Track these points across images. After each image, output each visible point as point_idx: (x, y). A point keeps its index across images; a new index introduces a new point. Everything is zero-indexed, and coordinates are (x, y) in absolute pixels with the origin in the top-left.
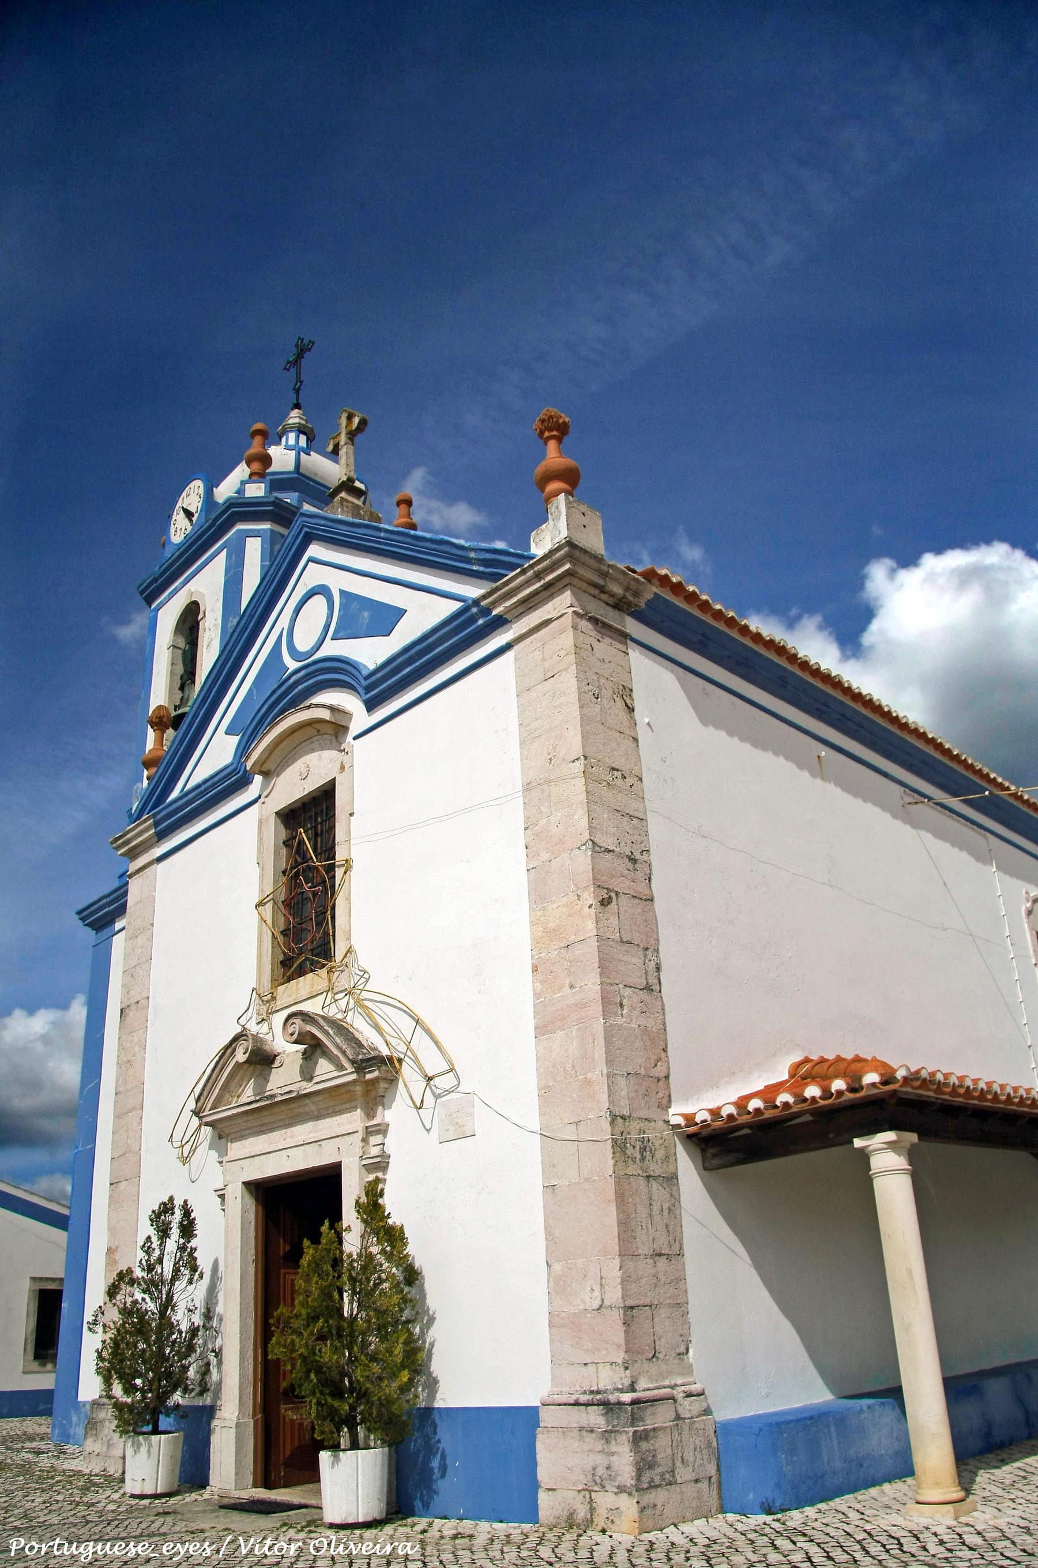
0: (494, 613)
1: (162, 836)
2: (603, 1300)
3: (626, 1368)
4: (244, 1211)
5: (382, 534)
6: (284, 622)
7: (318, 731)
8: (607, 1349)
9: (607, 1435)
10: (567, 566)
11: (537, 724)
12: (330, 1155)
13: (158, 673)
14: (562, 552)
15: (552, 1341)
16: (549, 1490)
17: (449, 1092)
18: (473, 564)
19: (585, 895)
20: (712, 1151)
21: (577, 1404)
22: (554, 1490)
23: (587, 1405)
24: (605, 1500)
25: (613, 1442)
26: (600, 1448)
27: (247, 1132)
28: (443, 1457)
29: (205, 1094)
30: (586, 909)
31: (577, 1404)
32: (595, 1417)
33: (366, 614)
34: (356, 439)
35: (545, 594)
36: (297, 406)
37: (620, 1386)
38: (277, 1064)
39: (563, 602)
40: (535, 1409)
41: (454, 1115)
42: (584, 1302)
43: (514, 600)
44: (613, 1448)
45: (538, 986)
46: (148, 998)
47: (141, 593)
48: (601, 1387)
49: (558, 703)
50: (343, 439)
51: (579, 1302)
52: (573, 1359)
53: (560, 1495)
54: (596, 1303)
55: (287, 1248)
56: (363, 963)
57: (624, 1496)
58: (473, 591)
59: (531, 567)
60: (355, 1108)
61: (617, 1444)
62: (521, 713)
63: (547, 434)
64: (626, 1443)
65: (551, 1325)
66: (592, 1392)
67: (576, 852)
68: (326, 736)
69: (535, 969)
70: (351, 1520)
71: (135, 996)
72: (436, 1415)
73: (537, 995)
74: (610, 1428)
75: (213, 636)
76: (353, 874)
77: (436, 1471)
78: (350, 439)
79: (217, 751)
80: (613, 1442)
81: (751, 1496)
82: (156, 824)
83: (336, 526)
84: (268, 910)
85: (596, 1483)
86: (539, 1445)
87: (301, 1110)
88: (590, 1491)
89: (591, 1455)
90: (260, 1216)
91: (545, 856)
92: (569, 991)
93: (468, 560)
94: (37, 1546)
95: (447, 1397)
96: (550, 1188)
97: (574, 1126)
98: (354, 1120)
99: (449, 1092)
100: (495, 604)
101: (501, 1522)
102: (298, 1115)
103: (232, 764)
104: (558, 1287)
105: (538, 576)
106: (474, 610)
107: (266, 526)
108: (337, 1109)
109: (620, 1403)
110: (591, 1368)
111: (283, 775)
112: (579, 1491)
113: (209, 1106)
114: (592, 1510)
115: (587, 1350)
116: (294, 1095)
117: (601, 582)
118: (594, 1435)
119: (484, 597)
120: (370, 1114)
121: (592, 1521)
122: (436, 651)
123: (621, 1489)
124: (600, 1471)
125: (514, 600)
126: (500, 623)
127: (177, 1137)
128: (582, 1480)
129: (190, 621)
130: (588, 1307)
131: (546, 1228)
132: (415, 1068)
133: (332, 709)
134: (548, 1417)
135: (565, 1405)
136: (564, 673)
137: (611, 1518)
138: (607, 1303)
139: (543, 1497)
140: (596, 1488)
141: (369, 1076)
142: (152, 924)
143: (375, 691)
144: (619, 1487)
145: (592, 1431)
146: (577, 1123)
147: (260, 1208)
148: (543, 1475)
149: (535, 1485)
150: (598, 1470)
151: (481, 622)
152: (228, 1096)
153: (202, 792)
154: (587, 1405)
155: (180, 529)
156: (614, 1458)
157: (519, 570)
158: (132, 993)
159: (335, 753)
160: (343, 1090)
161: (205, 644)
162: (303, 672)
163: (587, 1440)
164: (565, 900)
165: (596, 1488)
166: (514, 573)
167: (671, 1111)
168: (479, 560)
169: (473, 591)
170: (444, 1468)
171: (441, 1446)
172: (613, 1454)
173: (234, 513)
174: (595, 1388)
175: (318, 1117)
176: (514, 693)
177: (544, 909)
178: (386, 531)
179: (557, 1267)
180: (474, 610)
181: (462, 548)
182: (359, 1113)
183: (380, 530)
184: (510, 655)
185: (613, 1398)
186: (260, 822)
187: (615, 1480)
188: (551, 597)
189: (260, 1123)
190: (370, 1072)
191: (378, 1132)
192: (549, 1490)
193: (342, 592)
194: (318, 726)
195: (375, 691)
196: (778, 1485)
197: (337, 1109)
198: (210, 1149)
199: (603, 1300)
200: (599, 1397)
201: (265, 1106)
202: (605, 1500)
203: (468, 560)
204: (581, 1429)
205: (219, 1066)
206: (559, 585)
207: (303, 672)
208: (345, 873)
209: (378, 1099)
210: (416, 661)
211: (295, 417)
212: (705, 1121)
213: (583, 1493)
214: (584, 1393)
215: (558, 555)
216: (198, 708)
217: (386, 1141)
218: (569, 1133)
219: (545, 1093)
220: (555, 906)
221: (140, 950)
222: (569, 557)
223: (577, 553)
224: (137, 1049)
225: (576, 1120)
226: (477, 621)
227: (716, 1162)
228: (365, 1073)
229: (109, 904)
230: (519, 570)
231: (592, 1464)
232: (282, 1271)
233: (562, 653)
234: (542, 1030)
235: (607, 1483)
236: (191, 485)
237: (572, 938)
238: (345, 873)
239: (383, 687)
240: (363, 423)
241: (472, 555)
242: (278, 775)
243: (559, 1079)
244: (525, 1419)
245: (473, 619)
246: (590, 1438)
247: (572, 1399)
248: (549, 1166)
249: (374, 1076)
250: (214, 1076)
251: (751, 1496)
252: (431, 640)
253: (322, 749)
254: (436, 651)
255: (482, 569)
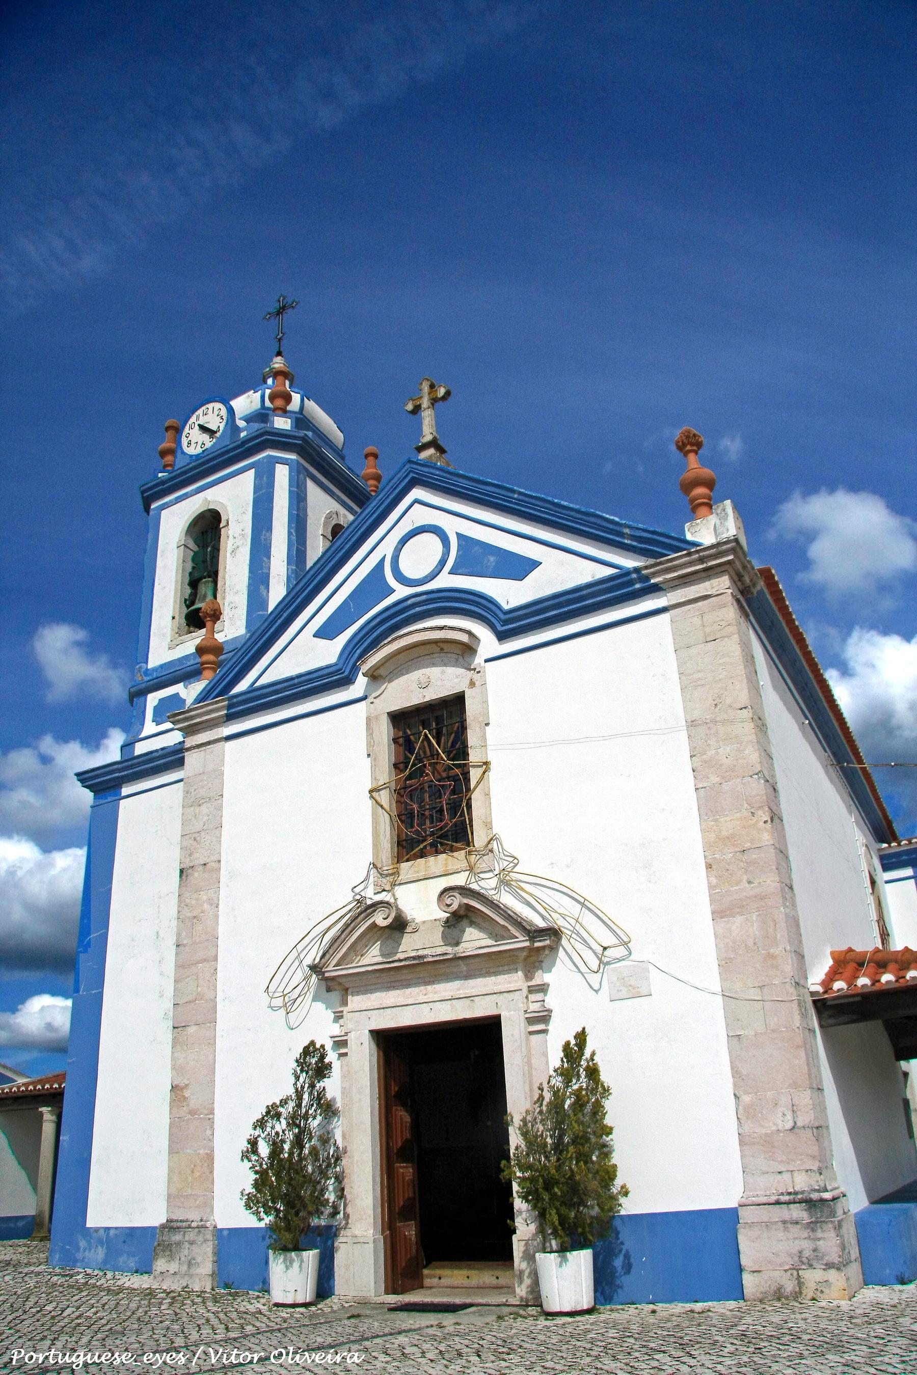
0: (652, 581)
1: (231, 717)
2: (795, 1123)
3: (821, 1174)
4: (371, 1055)
5: (516, 496)
6: (387, 549)
7: (442, 649)
8: (801, 1160)
9: (812, 1226)
10: (731, 557)
11: (700, 675)
12: (487, 1009)
13: (165, 567)
14: (729, 546)
15: (742, 1157)
16: (754, 1272)
17: (619, 960)
18: (624, 538)
19: (760, 812)
20: (827, 1013)
21: (778, 1203)
22: (759, 1271)
23: (788, 1203)
24: (813, 1276)
25: (819, 1230)
26: (806, 1235)
27: (373, 987)
28: (627, 1256)
29: (331, 951)
30: (761, 824)
31: (778, 1203)
32: (798, 1212)
33: (492, 559)
34: (437, 405)
35: (703, 575)
36: (279, 354)
37: (817, 1188)
38: (409, 929)
39: (722, 584)
40: (736, 1208)
41: (626, 979)
42: (775, 1124)
43: (676, 574)
44: (819, 1234)
45: (714, 881)
46: (219, 861)
47: (143, 492)
48: (797, 1188)
49: (721, 661)
50: (425, 403)
51: (771, 1124)
52: (765, 1169)
53: (765, 1275)
54: (789, 1125)
55: (397, 1089)
56: (509, 846)
57: (833, 1272)
58: (629, 562)
59: (697, 552)
60: (516, 971)
61: (823, 1231)
62: (681, 664)
63: (689, 448)
64: (832, 1230)
65: (742, 1143)
66: (790, 1194)
67: (749, 779)
68: (450, 655)
69: (709, 866)
70: (579, 1308)
71: (200, 857)
72: (617, 1223)
73: (711, 887)
74: (813, 1219)
75: (239, 543)
76: (492, 775)
77: (619, 1269)
78: (433, 404)
79: (304, 650)
80: (819, 1230)
81: (888, 1271)
82: (229, 707)
83: (455, 478)
84: (384, 797)
85: (803, 1263)
86: (741, 1239)
87: (455, 970)
88: (798, 1270)
89: (797, 1242)
90: (381, 1061)
91: (715, 779)
92: (747, 885)
93: (622, 535)
94: (250, 1356)
95: (629, 1207)
96: (734, 1038)
97: (758, 990)
98: (516, 980)
99: (619, 960)
100: (654, 574)
101: (696, 1302)
102: (453, 973)
103: (336, 664)
104: (745, 1114)
105: (701, 560)
106: (634, 576)
107: (293, 456)
108: (492, 970)
109: (822, 1200)
110: (787, 1176)
111: (396, 682)
112: (786, 1271)
113: (334, 962)
114: (800, 1284)
115: (782, 1162)
116: (451, 956)
117: (742, 572)
118: (799, 1226)
119: (646, 568)
120: (529, 976)
121: (801, 1293)
122: (587, 602)
123: (829, 1266)
124: (807, 1253)
125: (676, 574)
126: (656, 589)
127: (271, 989)
128: (788, 1262)
129: (207, 528)
130: (780, 1128)
131: (732, 1069)
132: (578, 939)
133: (469, 633)
134: (745, 1215)
135: (765, 1204)
136: (726, 639)
137: (820, 1289)
138: (799, 1124)
139: (747, 1278)
140: (803, 1267)
141: (537, 944)
142: (222, 795)
143: (514, 625)
144: (826, 1265)
145: (797, 1223)
146: (760, 987)
147: (381, 1053)
148: (744, 1261)
149: (741, 1269)
150: (804, 1252)
151: (638, 586)
152: (352, 954)
153: (295, 685)
154: (788, 1203)
155: (194, 442)
156: (821, 1242)
157: (685, 552)
158: (196, 855)
159: (461, 671)
160: (512, 953)
161: (230, 548)
162: (424, 597)
163: (792, 1230)
164: (738, 815)
165: (803, 1267)
166: (676, 555)
167: (810, 981)
168: (632, 535)
169: (629, 562)
170: (628, 1267)
171: (624, 1248)
172: (819, 1239)
173: (268, 440)
174: (791, 1190)
175: (467, 977)
176: (672, 649)
177: (716, 820)
178: (520, 493)
179: (746, 1099)
180: (634, 576)
181: (617, 523)
182: (520, 973)
183: (513, 491)
184: (665, 617)
185: (815, 1196)
186: (369, 720)
187: (822, 1258)
188: (709, 578)
189: (393, 980)
190: (540, 941)
191: (538, 991)
192: (754, 1272)
193: (459, 535)
194: (441, 645)
195: (514, 625)
196: (905, 1262)
197: (492, 970)
198: (314, 999)
199: (795, 1123)
200: (800, 1196)
201: (409, 965)
202: (813, 1276)
203: (622, 535)
204: (784, 1222)
205: (350, 928)
206: (716, 570)
207: (424, 597)
208: (484, 773)
209: (537, 964)
210: (564, 607)
211: (278, 363)
212: (842, 989)
213: (789, 1273)
214: (782, 1194)
215: (724, 547)
216: (282, 610)
217: (546, 999)
218: (754, 994)
219: (726, 965)
220: (728, 818)
221: (206, 818)
222: (733, 551)
223: (738, 549)
224: (206, 906)
225: (760, 985)
226: (634, 585)
227: (831, 1021)
228: (534, 942)
229: (119, 770)
230: (685, 552)
231: (797, 1248)
232: (394, 1108)
233: (723, 624)
234: (718, 914)
235: (815, 1263)
236: (210, 406)
237: (748, 845)
238: (484, 773)
239: (512, 624)
240: (448, 393)
241: (627, 531)
242: (390, 681)
243: (740, 952)
244: (727, 1219)
245: (631, 583)
246: (795, 1230)
247: (773, 1199)
248: (731, 1019)
249: (539, 945)
250: (343, 936)
251: (888, 1271)
252: (584, 592)
253: (445, 665)
254: (587, 602)
255: (634, 543)
